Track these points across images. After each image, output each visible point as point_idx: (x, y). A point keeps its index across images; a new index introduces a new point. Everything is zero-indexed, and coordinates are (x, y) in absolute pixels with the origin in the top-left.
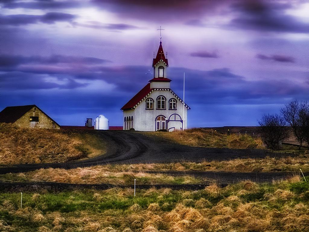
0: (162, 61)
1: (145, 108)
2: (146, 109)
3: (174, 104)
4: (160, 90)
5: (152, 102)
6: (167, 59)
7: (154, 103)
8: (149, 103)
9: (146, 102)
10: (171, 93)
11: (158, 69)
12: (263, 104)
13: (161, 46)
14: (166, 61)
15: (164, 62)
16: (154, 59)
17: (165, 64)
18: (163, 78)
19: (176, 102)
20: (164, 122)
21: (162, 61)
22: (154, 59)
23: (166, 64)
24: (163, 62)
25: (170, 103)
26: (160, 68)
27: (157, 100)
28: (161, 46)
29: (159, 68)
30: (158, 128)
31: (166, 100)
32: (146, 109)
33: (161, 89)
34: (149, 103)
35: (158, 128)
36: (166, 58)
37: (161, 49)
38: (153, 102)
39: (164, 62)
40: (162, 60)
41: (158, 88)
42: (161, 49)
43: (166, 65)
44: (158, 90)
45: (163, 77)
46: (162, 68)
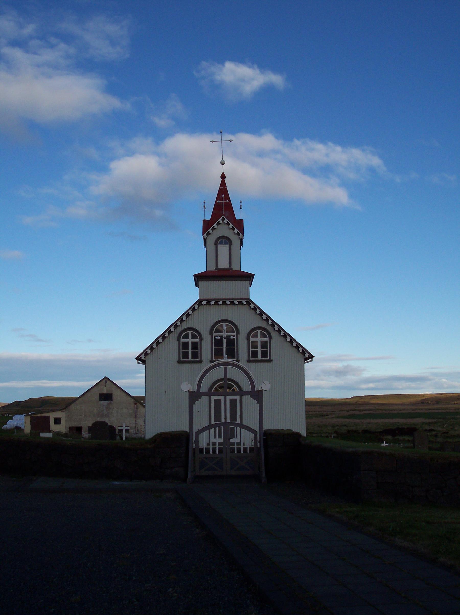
0: (226, 220)
1: (177, 359)
2: (179, 362)
3: (195, 346)
4: (220, 302)
5: (267, 339)
6: (241, 221)
7: (203, 342)
8: (188, 343)
9: (179, 339)
10: (258, 316)
11: (215, 246)
12: (40, 380)
13: (223, 184)
14: (239, 225)
15: (231, 225)
16: (204, 221)
17: (233, 229)
18: (229, 270)
19: (271, 338)
20: (236, 400)
21: (226, 220)
22: (204, 221)
23: (236, 231)
24: (228, 224)
25: (183, 343)
26: (221, 243)
27: (211, 333)
28: (223, 184)
29: (216, 243)
30: (218, 417)
31: (238, 333)
32: (179, 362)
33: (221, 300)
34: (188, 343)
35: (218, 417)
36: (237, 218)
37: (223, 190)
38: (201, 339)
39: (231, 225)
40: (223, 219)
41: (221, 300)
42: (223, 190)
43: (238, 234)
44: (212, 302)
45: (227, 266)
46: (226, 243)
